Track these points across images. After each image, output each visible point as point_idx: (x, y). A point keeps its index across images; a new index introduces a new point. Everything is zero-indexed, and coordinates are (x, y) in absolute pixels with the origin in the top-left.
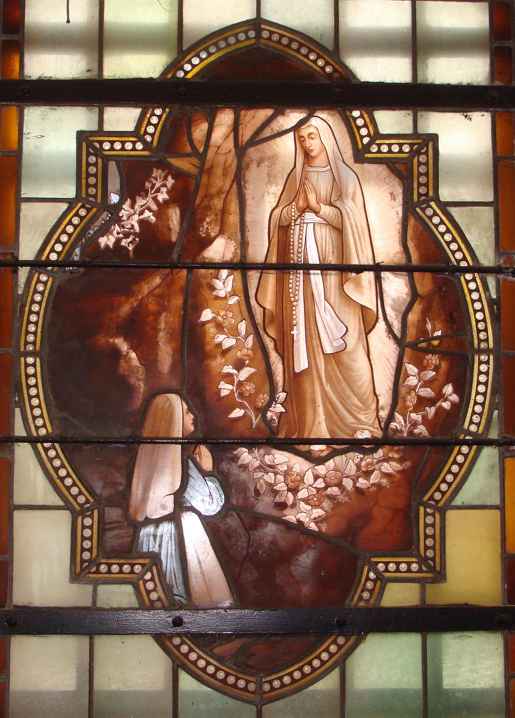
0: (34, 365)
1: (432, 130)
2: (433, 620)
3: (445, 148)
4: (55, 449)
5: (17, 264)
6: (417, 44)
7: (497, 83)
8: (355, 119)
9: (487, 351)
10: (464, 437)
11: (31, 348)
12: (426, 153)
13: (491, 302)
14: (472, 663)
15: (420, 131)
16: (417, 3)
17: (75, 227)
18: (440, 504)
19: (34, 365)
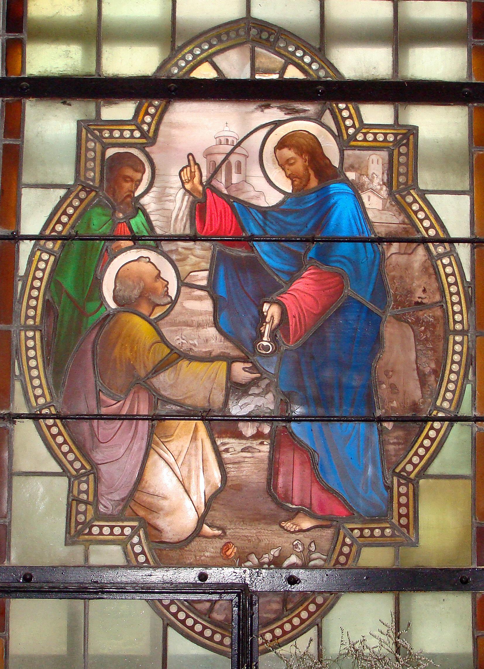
0: (33, 338)
1: (412, 122)
2: (406, 581)
3: (424, 134)
4: (57, 426)
5: (17, 238)
6: (400, 36)
7: (474, 81)
8: (341, 111)
9: (34, 328)
10: (437, 414)
11: (31, 322)
12: (77, 523)
13: (466, 285)
14: (442, 624)
15: (401, 122)
16: (400, 4)
17: (76, 208)
18: (412, 476)
19: (33, 338)
